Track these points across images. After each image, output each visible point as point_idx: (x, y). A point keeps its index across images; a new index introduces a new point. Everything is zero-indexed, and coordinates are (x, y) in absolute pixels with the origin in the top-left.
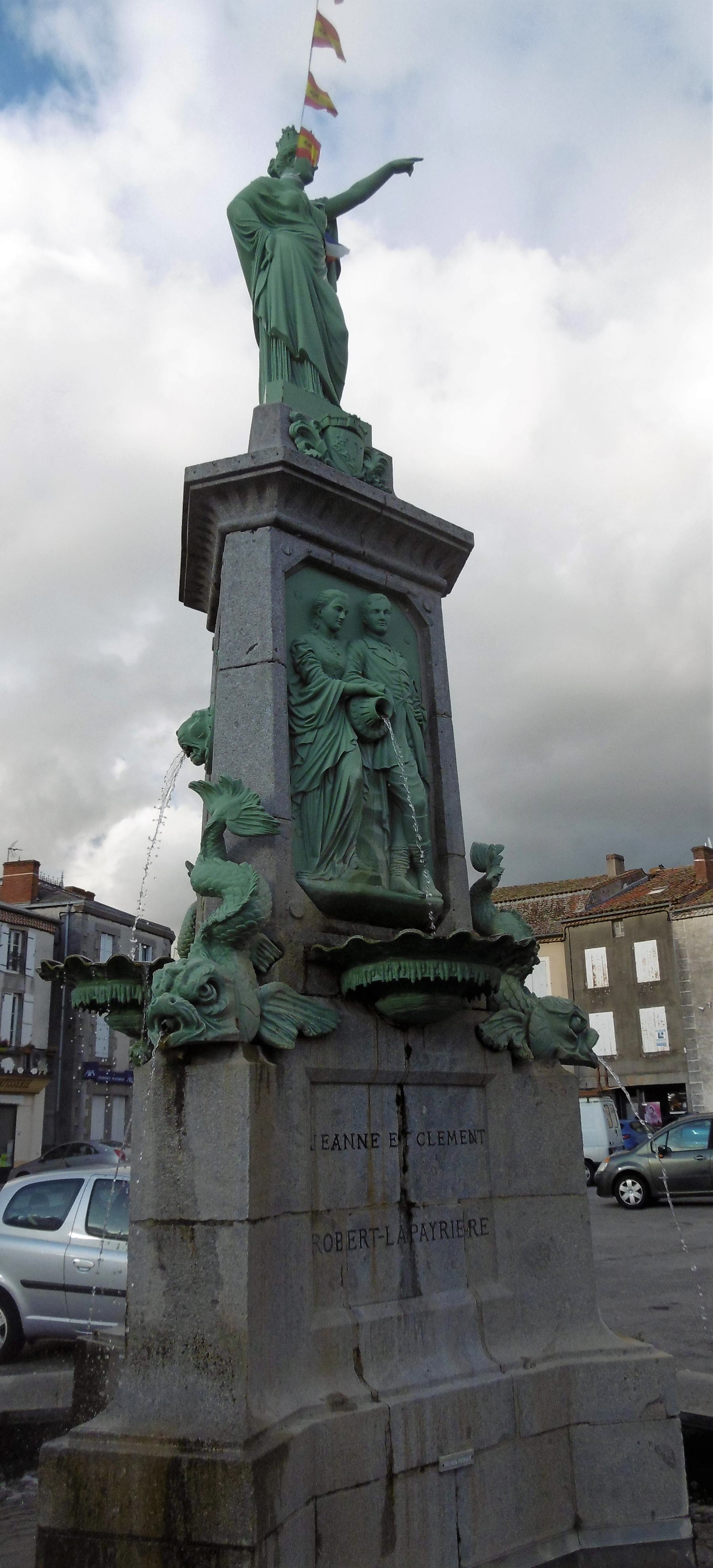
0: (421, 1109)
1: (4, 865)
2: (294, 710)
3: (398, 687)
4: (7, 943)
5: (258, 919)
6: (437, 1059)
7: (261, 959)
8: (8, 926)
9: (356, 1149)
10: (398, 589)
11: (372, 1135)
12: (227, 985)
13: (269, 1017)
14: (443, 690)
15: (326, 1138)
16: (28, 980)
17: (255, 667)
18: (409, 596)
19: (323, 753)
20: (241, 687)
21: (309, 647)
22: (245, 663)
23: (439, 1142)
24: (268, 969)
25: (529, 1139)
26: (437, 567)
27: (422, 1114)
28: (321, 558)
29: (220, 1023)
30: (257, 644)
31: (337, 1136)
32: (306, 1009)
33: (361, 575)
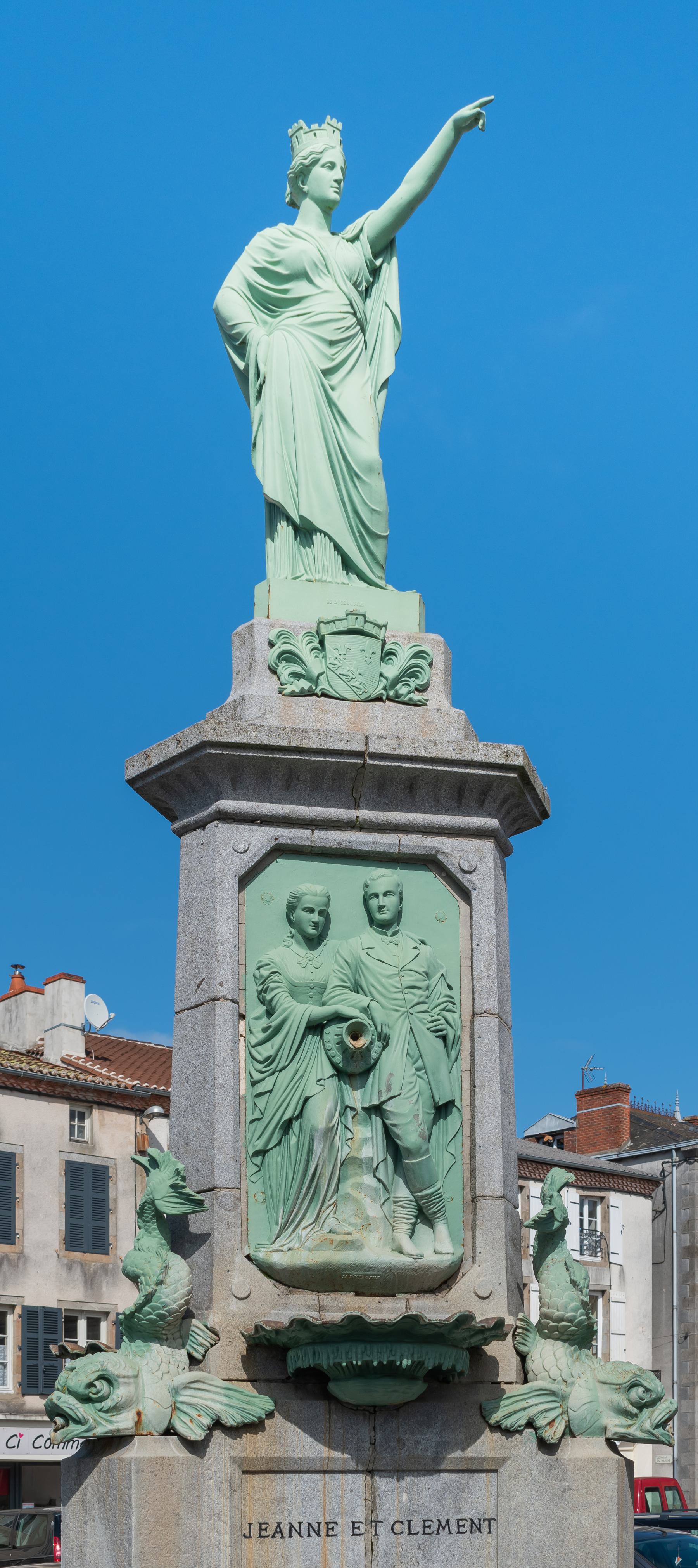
0: (399, 1496)
1: (576, 1095)
2: (253, 1051)
3: (400, 996)
4: (578, 1217)
5: (167, 1308)
6: (418, 1442)
7: (195, 1346)
8: (577, 1193)
9: (306, 1538)
10: (422, 852)
11: (327, 1523)
12: (120, 1380)
13: (184, 1408)
14: (485, 980)
15: (264, 1526)
16: (615, 1269)
17: (201, 1008)
18: (440, 856)
19: (284, 1101)
20: (191, 1033)
21: (272, 968)
22: (193, 1004)
23: (424, 1531)
24: (204, 1356)
25: (552, 1529)
26: (481, 802)
27: (401, 1502)
28: (296, 842)
29: (114, 1419)
30: (204, 979)
31: (279, 1524)
32: (230, 1397)
33: (358, 848)
